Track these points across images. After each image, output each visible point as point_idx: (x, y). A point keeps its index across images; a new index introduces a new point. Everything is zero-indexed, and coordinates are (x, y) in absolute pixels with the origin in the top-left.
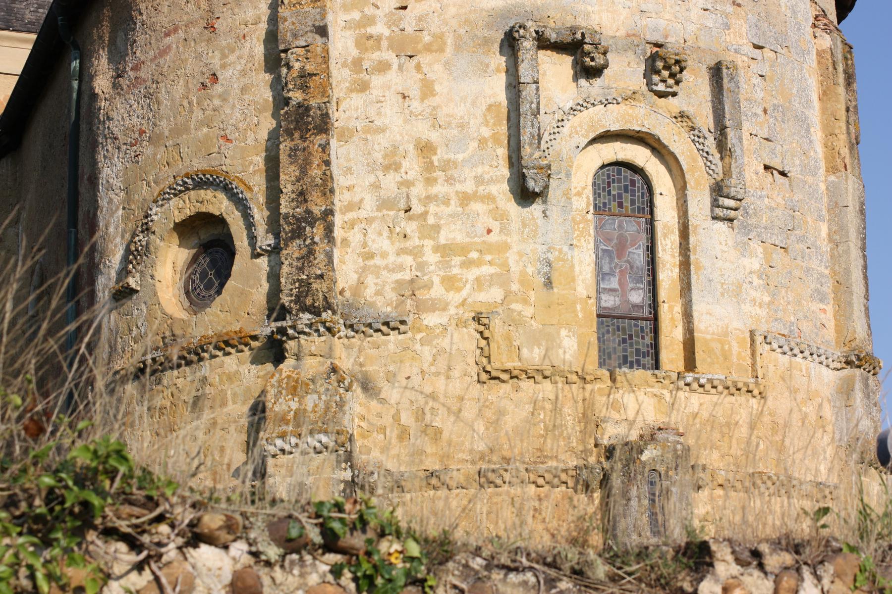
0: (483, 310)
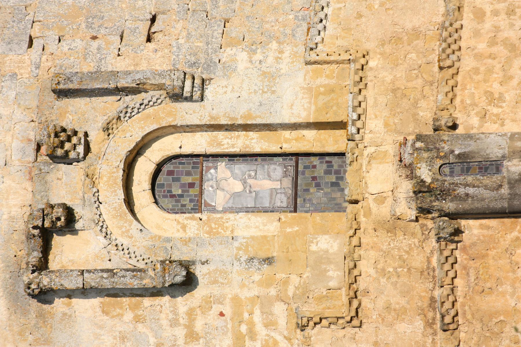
0: (295, 321)
